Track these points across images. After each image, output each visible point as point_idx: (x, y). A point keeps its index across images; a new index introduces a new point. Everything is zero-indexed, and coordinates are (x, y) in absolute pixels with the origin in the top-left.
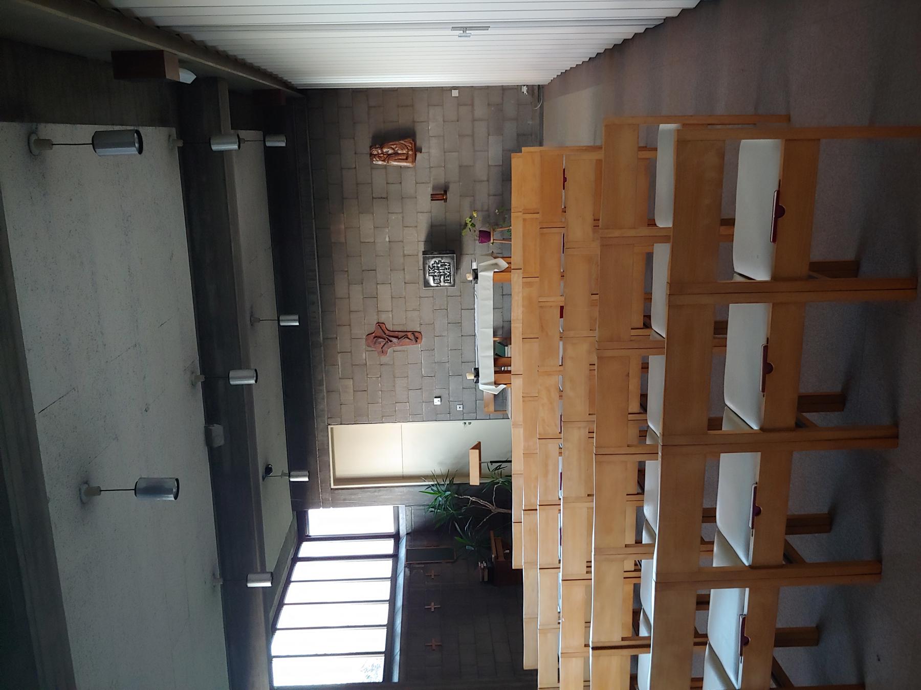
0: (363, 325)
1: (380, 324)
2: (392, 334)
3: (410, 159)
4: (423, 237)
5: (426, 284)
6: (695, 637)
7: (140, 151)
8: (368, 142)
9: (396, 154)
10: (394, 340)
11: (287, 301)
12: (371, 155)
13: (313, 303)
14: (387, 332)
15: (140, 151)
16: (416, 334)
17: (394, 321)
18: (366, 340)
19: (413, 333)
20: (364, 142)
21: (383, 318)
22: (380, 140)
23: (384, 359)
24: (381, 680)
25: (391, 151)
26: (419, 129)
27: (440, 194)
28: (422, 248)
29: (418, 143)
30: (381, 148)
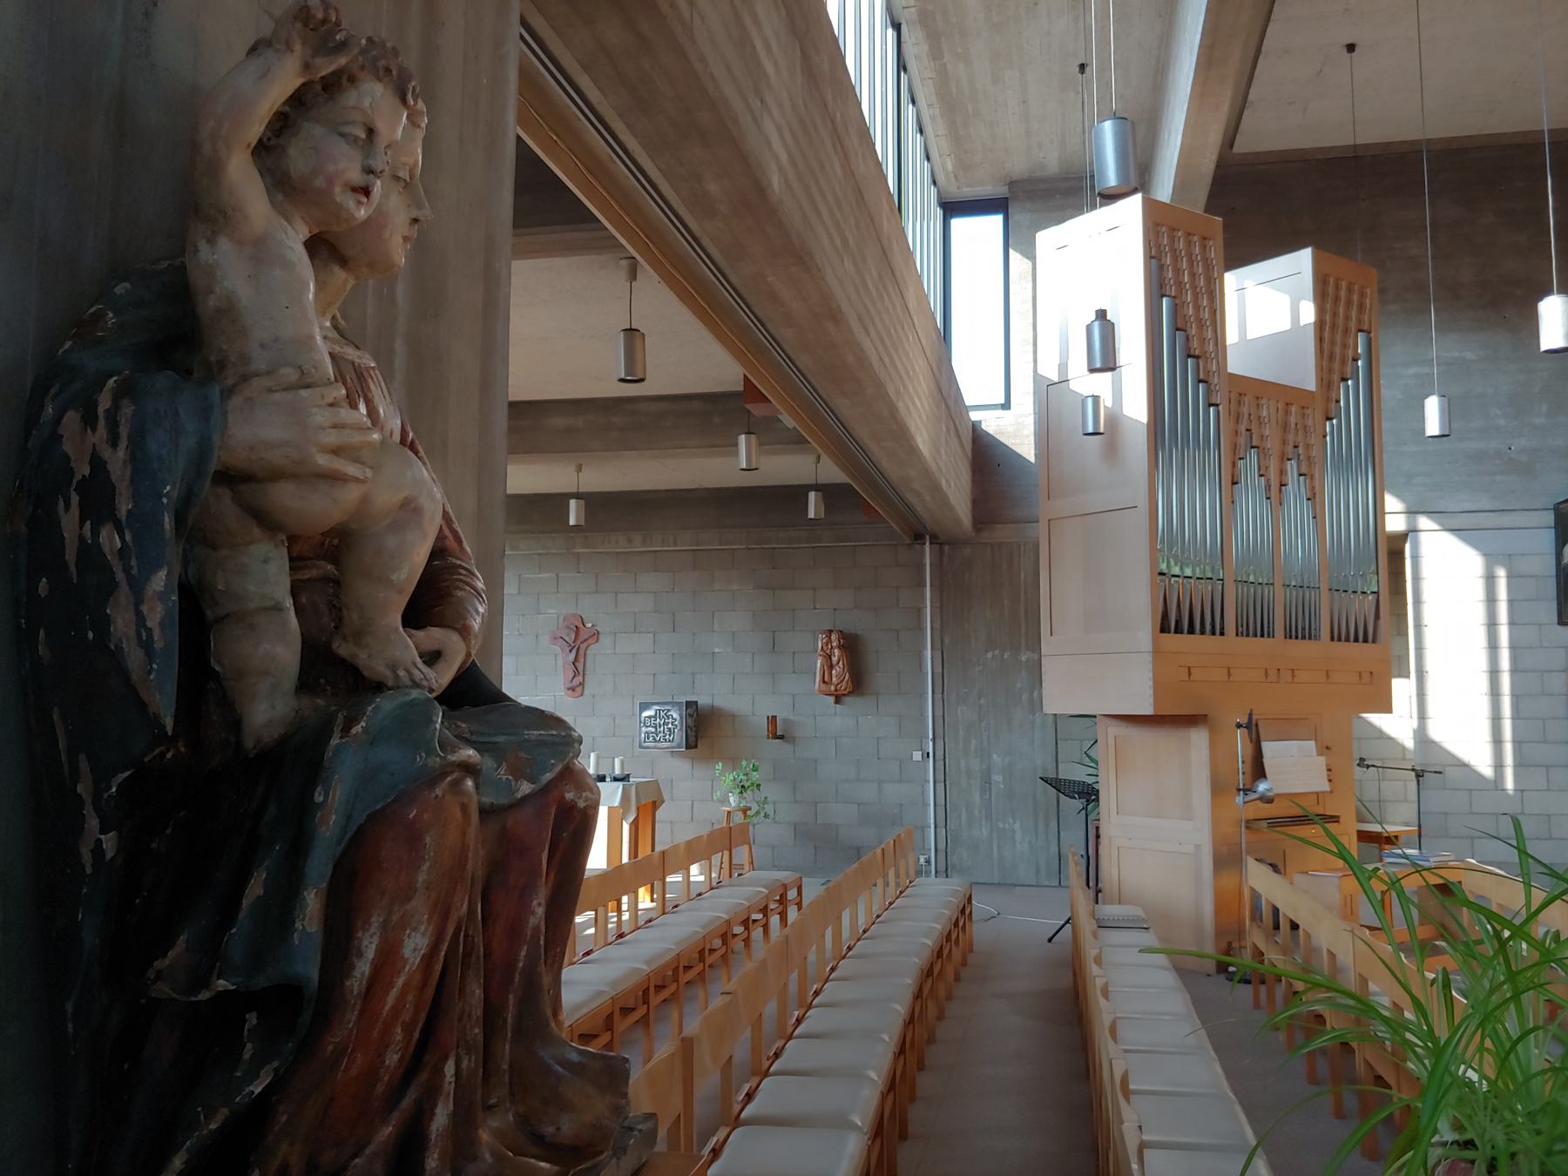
0: (595, 611)
1: (596, 635)
2: (582, 652)
3: (824, 687)
4: (720, 702)
5: (645, 706)
6: (1317, 638)
7: (622, 380)
8: (849, 628)
9: (831, 667)
10: (572, 657)
11: (610, 510)
12: (830, 631)
13: (630, 541)
14: (583, 646)
15: (622, 380)
16: (579, 690)
17: (597, 655)
18: (574, 615)
19: (582, 684)
20: (855, 622)
21: (605, 640)
22: (852, 646)
23: (545, 640)
24: (509, 468)
25: (835, 659)
26: (711, 757)
27: (777, 731)
28: (703, 700)
29: (847, 699)
30: (839, 647)
